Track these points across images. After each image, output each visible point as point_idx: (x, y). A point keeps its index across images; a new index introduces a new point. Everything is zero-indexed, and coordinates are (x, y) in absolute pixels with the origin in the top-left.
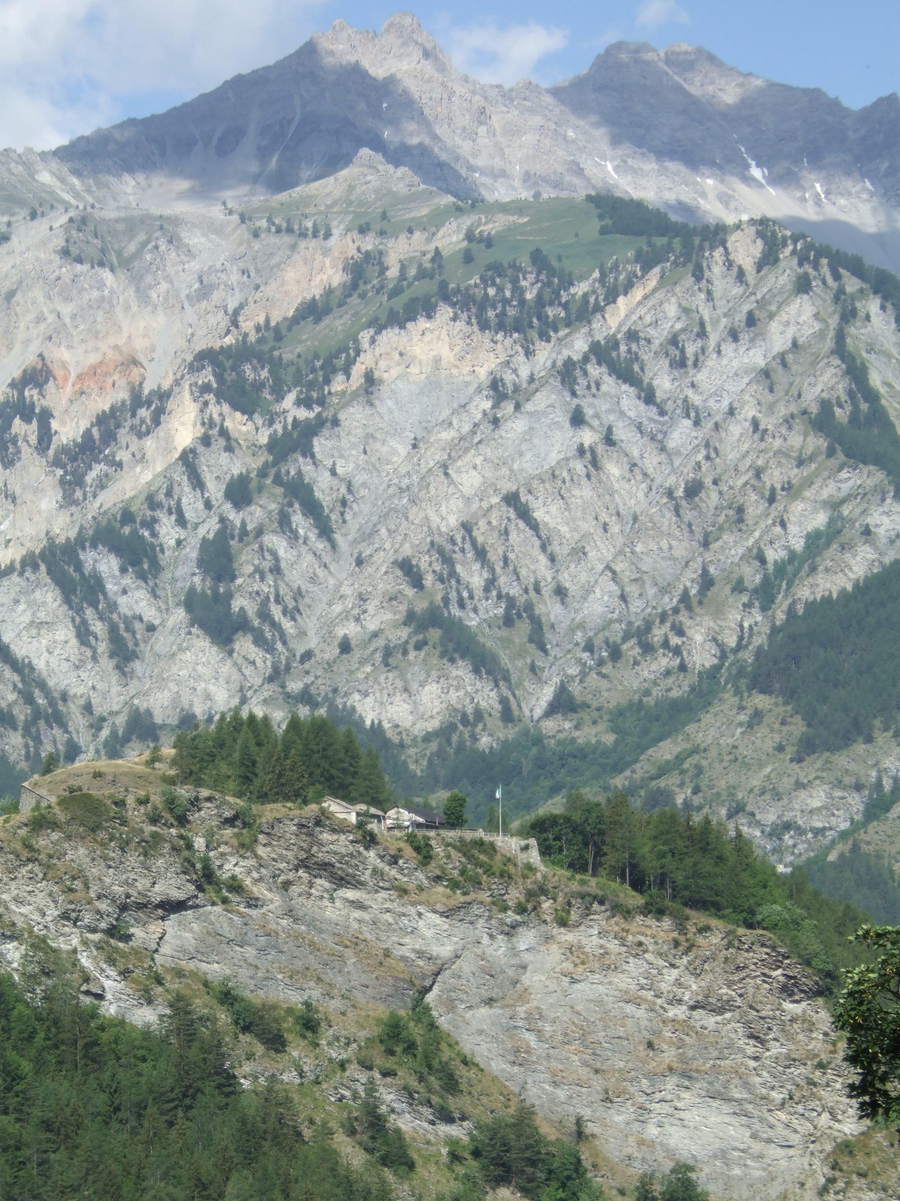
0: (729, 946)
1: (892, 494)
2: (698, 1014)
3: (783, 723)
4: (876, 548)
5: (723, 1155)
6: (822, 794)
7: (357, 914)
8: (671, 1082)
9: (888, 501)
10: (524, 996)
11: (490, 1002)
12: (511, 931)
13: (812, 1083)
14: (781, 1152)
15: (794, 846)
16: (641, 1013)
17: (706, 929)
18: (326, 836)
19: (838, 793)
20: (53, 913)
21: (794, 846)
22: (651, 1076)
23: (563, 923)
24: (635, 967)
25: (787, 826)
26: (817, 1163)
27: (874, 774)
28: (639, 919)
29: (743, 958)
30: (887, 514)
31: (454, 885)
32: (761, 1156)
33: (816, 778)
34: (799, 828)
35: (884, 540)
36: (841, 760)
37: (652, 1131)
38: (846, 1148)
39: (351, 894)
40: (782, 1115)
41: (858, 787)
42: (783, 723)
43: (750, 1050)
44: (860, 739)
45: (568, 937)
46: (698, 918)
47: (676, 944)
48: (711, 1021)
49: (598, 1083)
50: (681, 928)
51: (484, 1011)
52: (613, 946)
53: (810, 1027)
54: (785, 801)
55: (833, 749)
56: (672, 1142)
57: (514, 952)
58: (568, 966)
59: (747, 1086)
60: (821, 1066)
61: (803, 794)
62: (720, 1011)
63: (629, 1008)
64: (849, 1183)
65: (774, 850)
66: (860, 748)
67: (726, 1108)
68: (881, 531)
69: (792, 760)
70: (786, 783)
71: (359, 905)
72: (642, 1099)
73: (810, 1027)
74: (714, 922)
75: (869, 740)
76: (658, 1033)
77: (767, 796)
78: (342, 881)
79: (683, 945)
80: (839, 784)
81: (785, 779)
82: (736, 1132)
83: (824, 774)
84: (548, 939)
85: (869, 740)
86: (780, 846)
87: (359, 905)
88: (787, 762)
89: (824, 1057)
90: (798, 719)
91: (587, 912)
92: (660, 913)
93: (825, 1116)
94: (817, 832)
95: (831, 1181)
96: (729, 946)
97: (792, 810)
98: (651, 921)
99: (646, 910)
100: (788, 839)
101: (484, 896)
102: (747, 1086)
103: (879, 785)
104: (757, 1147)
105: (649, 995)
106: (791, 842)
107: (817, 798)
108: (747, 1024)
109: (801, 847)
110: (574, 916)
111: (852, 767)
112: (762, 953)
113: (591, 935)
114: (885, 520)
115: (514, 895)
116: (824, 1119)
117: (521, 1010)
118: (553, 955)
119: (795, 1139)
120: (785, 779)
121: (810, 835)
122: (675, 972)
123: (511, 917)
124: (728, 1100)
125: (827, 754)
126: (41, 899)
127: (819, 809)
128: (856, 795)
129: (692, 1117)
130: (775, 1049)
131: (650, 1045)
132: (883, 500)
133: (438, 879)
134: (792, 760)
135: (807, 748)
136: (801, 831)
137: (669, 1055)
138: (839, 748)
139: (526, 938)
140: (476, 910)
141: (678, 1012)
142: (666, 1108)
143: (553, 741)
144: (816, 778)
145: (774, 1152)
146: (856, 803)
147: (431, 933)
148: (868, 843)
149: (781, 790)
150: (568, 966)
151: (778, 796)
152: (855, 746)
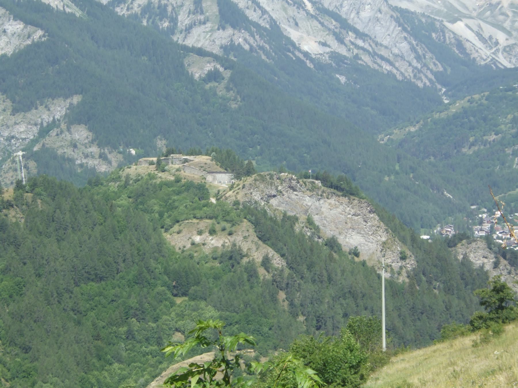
0: (359, 203)
1: (12, 18)
2: (354, 216)
3: (4, 101)
4: (8, 37)
5: (360, 245)
6: (24, 127)
7: (296, 197)
8: (351, 230)
9: (11, 21)
10: (323, 213)
11: (317, 214)
12: (319, 200)
13: (376, 230)
14: (371, 244)
15: (16, 144)
16: (343, 216)
17: (354, 199)
18: (292, 181)
19: (29, 127)
20: (260, 198)
21: (16, 144)
22: (347, 229)
23: (328, 198)
24: (341, 207)
25: (13, 137)
26: (378, 246)
27: (40, 120)
28: (341, 197)
29: (362, 205)
30: (11, 25)
31: (310, 191)
32: (367, 245)
33: (22, 121)
34: (17, 138)
35: (10, 35)
36: (29, 115)
37: (347, 240)
38: (384, 243)
39: (295, 193)
40: (372, 237)
41: (36, 125)
42: (4, 101)
43: (364, 224)
44: (34, 108)
45: (329, 201)
46: (352, 197)
47: (349, 202)
48: (356, 218)
49: (337, 230)
50: (349, 199)
51: (316, 216)
52: (337, 203)
53: (375, 219)
54: (11, 129)
55: (25, 112)
56: (351, 242)
57: (320, 204)
58: (329, 207)
59: (364, 231)
60: (378, 227)
61: (17, 126)
62: (358, 216)
63: (341, 215)
64: (386, 250)
65: (8, 145)
66: (34, 111)
67: (360, 235)
68: (9, 31)
69: (11, 115)
70: (10, 123)
71: (297, 195)
72: (345, 234)
73: (375, 219)
74: (355, 198)
75: (36, 108)
76: (346, 220)
77: (5, 127)
78: (295, 190)
79: (350, 203)
80: (29, 123)
81: (10, 121)
82: (362, 240)
83: (24, 120)
84: (325, 201)
85: (36, 108)
86: (10, 144)
87: (297, 195)
88: (9, 116)
89: (378, 225)
90: (8, 100)
91: (332, 196)
92: (345, 196)
93: (379, 237)
94: (23, 139)
95: (383, 250)
96: (359, 203)
97: (14, 132)
98: (344, 198)
99: (342, 196)
100: (13, 141)
101: (315, 193)
102: (364, 231)
103: (42, 123)
104: (367, 243)
105: (344, 213)
106: (14, 143)
107: (22, 128)
108: (364, 219)
109: (18, 144)
110: (330, 197)
111: (33, 118)
112: (366, 204)
113: (332, 201)
114: (10, 27)
115: (320, 193)
116: (379, 237)
117: (323, 216)
118: (327, 205)
119: (374, 241)
120: (10, 121)
121: (21, 140)
122: (349, 208)
123: (320, 197)
124: (360, 234)
125: (23, 113)
126: (258, 195)
127: (23, 132)
128: (35, 127)
129: (354, 237)
130: (369, 224)
131: (346, 223)
132: (9, 20)
133: (307, 190)
134: (11, 115)
135: (15, 111)
136: (18, 139)
137: (349, 225)
138: (27, 111)
139: (322, 201)
140: (314, 196)
141: (350, 216)
142: (350, 235)
143: (80, 130)
144: (22, 121)
145: (370, 244)
146: (35, 130)
147: (308, 201)
148: (47, 144)
149: (9, 125)
150: (329, 207)
151: (8, 127)
152: (32, 110)
